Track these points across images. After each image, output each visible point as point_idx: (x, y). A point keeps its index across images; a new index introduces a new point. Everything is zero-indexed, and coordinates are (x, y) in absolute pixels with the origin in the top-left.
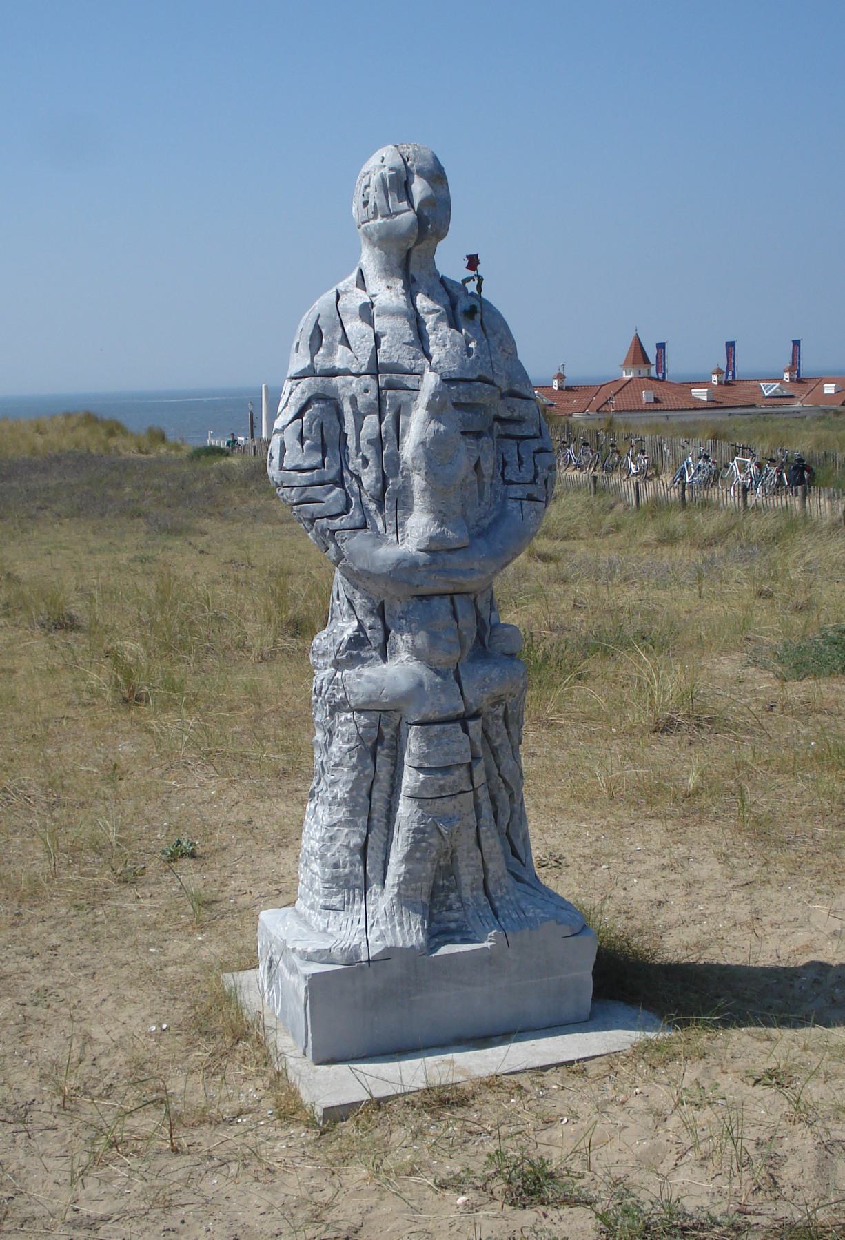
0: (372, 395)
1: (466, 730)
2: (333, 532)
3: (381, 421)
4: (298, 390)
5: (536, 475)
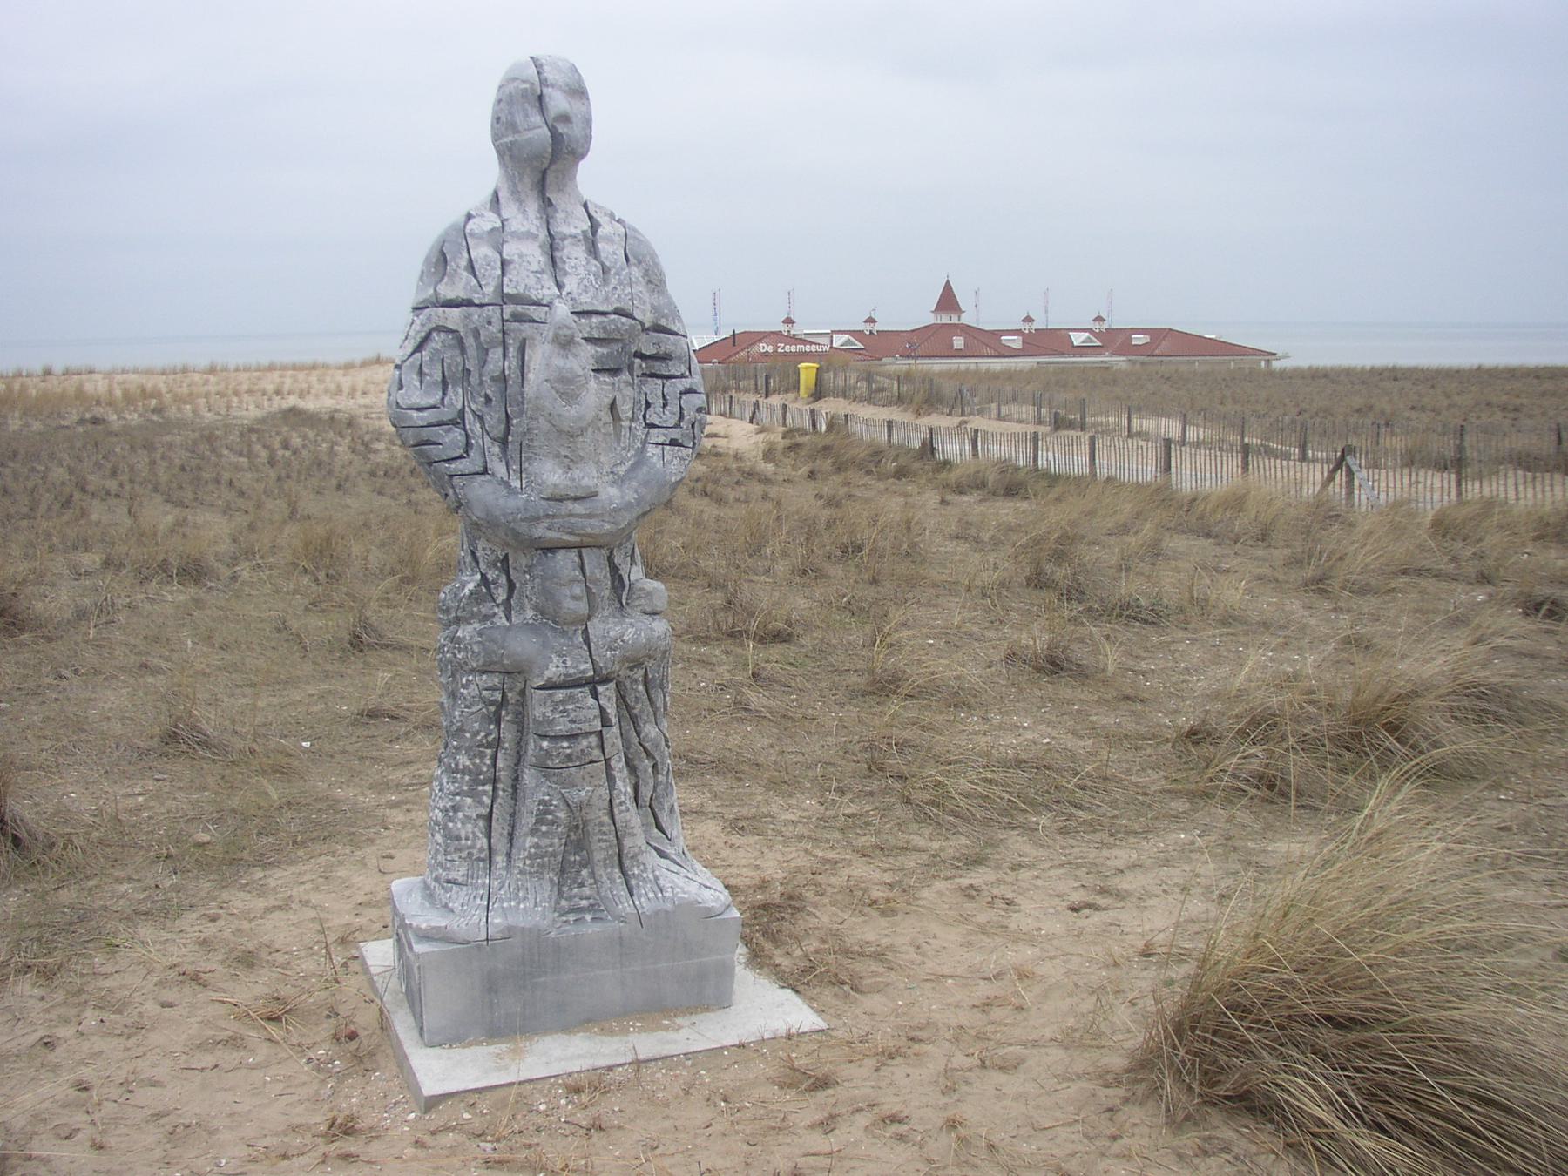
0: (495, 329)
1: (595, 695)
2: (451, 476)
3: (505, 356)
4: (418, 322)
5: (682, 417)
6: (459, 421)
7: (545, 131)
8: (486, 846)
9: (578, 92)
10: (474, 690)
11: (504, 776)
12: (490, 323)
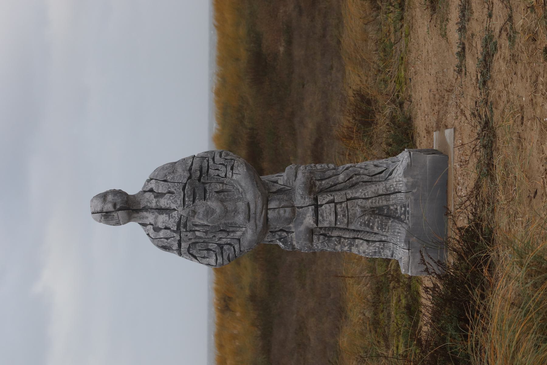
0: (189, 234)
2: (240, 251)
6: (221, 246)
7: (120, 213)
8: (378, 243)
9: (104, 196)
10: (319, 245)
11: (352, 235)
12: (187, 235)
